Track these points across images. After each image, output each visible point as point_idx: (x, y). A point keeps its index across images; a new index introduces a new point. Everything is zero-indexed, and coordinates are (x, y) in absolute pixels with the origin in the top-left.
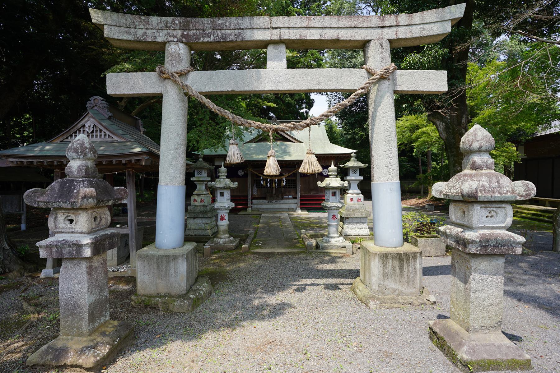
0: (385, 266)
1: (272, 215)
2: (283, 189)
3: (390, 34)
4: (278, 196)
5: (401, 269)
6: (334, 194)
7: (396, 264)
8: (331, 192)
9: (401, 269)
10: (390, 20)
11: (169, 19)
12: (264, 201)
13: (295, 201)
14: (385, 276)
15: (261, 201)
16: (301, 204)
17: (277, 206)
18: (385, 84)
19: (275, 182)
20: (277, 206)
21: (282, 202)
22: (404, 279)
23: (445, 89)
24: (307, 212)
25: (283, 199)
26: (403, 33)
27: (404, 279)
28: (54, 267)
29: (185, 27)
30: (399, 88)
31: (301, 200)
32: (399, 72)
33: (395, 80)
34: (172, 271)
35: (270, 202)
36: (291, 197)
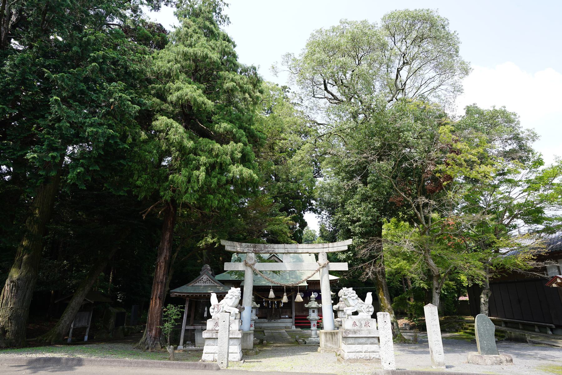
0: (326, 337)
1: (272, 331)
2: (280, 310)
3: (326, 250)
4: (276, 316)
5: (332, 338)
6: (314, 312)
7: (330, 336)
8: (312, 310)
9: (332, 338)
10: (326, 245)
11: (249, 244)
12: (265, 320)
13: (290, 320)
14: (327, 341)
15: (262, 320)
16: (296, 323)
17: (275, 325)
18: (325, 269)
19: (275, 304)
20: (275, 325)
21: (279, 321)
22: (334, 342)
23: (347, 269)
24: (300, 329)
25: (280, 318)
26: (331, 250)
27: (334, 342)
28: (183, 345)
29: (255, 247)
30: (331, 270)
31: (296, 319)
32: (330, 263)
33: (328, 267)
34: (248, 340)
35: (270, 321)
36: (287, 316)
